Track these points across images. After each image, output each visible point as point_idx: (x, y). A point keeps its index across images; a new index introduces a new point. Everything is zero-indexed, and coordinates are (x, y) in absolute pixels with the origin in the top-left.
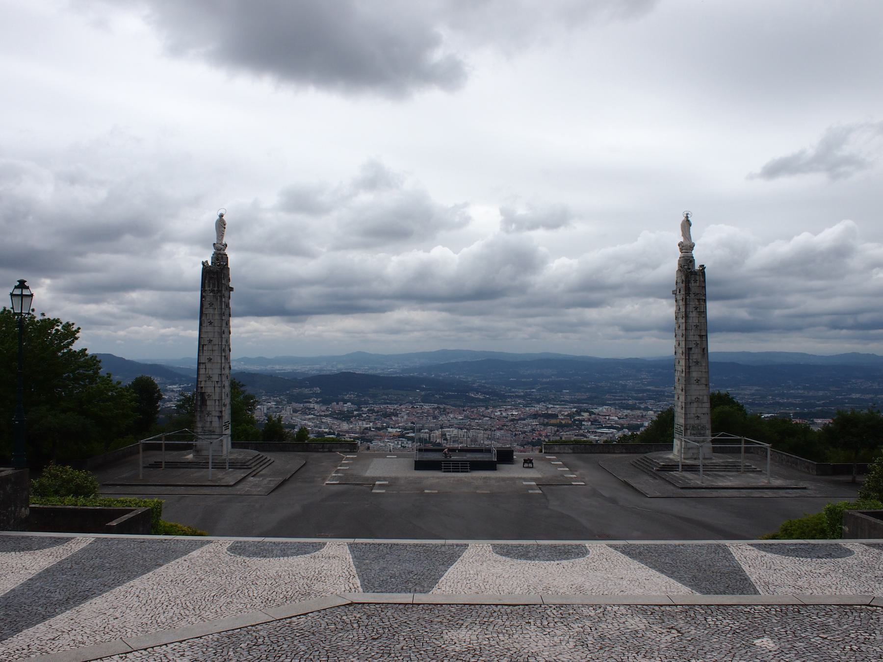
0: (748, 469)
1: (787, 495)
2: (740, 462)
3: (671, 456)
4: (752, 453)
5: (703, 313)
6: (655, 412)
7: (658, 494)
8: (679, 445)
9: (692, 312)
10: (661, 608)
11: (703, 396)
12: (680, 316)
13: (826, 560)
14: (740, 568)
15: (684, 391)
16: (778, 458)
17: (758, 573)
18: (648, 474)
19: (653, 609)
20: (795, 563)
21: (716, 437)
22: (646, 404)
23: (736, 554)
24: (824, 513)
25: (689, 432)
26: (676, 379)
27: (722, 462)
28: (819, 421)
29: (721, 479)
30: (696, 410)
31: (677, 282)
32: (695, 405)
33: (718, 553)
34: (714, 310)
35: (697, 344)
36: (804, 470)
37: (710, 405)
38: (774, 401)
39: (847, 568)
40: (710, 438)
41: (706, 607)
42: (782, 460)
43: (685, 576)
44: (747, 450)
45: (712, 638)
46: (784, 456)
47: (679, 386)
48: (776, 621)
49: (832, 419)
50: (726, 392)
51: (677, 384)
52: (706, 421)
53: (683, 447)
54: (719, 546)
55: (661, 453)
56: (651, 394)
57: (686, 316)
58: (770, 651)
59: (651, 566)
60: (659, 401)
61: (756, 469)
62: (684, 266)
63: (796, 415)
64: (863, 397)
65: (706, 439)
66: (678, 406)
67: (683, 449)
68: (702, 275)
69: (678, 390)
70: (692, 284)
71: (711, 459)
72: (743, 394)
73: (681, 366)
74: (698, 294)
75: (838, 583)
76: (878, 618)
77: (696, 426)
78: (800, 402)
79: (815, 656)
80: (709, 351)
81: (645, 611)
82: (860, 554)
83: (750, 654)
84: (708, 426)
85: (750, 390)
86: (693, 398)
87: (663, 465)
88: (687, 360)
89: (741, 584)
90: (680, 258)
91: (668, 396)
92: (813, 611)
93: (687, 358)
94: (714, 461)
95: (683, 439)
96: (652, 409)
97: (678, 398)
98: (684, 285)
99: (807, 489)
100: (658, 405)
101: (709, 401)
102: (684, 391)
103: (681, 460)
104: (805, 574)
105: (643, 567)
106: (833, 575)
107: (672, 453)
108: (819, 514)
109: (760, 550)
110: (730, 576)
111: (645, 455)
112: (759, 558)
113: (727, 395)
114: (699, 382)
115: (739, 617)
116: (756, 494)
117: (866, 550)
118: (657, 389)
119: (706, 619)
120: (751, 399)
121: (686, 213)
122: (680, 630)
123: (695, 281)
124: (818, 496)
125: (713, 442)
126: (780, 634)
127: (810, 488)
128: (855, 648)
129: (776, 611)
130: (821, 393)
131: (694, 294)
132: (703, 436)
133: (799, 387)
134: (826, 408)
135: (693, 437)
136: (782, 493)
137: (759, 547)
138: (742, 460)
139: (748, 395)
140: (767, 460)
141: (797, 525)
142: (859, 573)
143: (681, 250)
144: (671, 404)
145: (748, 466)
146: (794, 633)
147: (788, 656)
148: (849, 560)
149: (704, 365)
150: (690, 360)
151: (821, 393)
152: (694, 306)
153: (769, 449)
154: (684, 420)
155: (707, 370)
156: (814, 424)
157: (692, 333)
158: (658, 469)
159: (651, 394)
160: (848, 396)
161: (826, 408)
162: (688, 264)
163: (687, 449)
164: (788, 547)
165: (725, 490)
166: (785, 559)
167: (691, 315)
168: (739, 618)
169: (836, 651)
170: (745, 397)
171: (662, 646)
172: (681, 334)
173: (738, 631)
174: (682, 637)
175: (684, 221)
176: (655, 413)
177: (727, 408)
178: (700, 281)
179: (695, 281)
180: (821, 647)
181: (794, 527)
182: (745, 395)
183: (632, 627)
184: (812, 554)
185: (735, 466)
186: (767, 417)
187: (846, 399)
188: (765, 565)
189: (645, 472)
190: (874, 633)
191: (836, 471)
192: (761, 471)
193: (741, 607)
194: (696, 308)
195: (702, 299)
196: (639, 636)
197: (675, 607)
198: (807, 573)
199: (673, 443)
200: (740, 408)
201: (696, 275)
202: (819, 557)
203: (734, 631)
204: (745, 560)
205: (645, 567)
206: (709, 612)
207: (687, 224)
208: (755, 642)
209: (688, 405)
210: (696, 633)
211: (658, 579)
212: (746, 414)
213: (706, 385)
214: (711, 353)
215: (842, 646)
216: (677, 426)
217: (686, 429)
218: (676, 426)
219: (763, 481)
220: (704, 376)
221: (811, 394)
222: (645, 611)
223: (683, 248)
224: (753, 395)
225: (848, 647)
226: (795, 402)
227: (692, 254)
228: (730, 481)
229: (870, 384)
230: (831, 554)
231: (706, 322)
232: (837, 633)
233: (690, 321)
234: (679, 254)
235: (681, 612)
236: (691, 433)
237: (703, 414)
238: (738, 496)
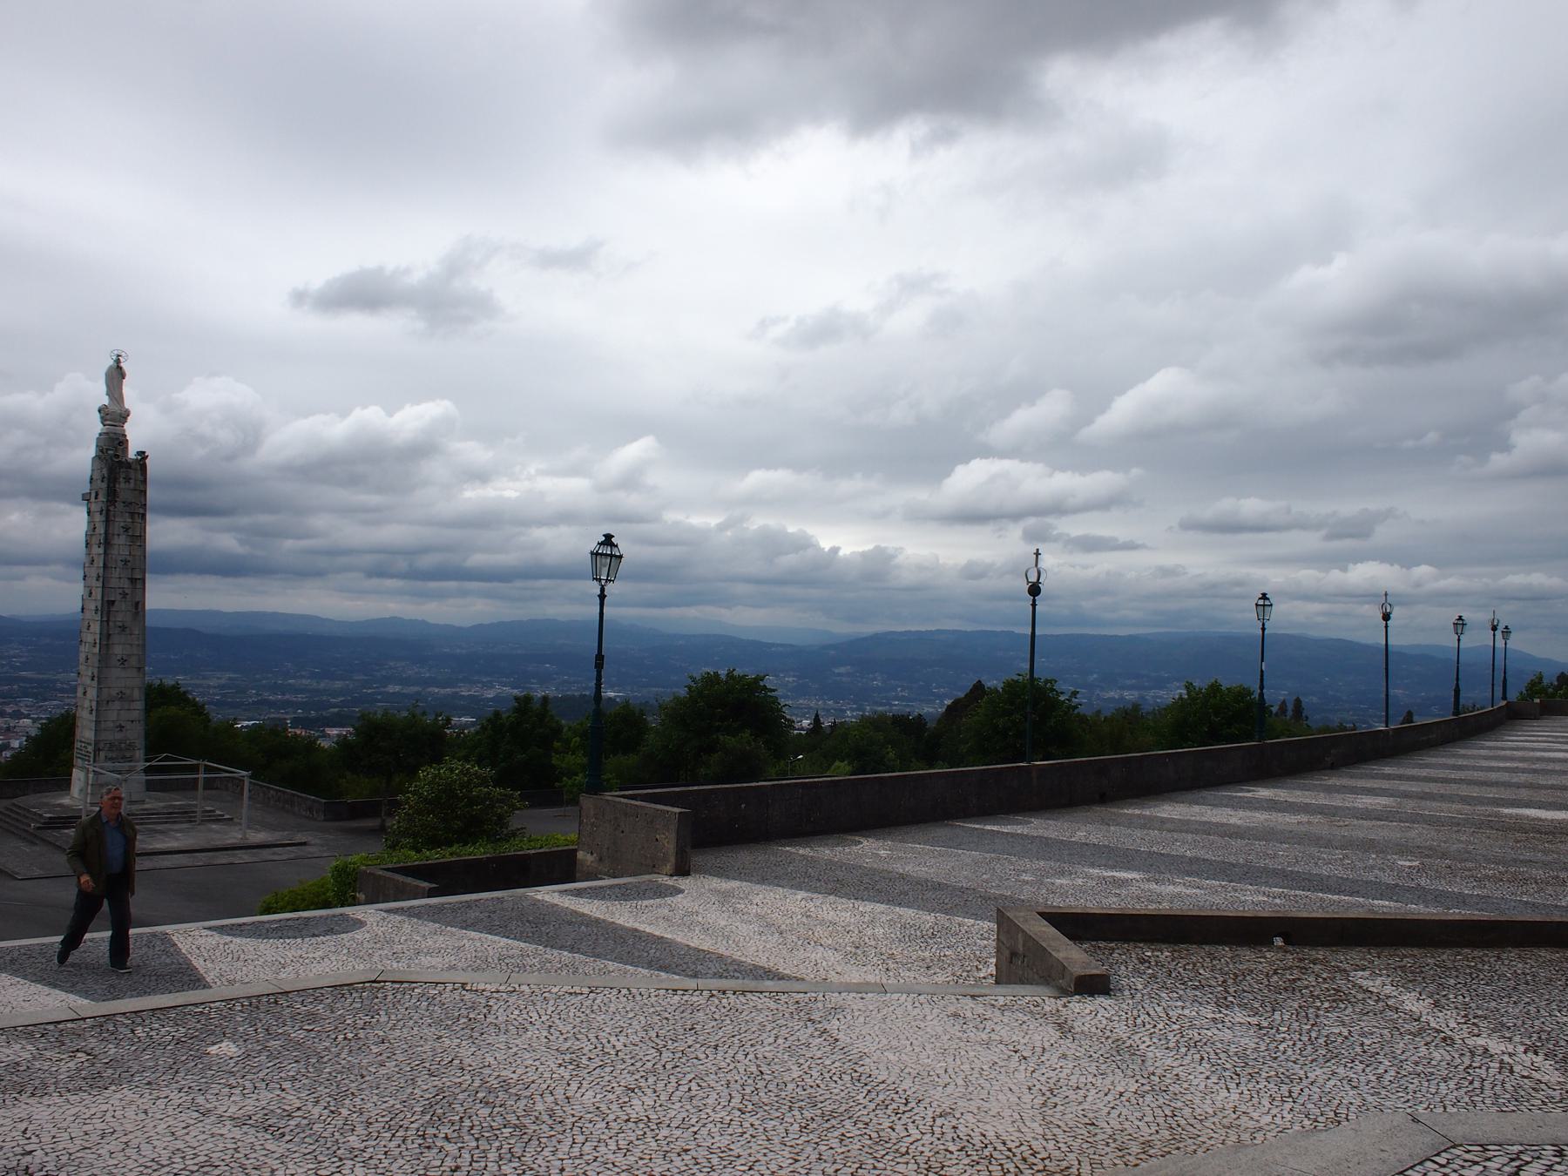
0: (210, 816)
1: (276, 858)
2: (196, 806)
3: (66, 801)
4: (217, 788)
5: (139, 539)
6: (34, 720)
7: (37, 872)
8: (82, 779)
9: (119, 535)
10: (59, 1026)
11: (133, 688)
12: (94, 540)
13: (325, 939)
14: (189, 963)
15: (96, 679)
16: (261, 795)
17: (218, 968)
18: (13, 833)
19: (45, 1029)
20: (277, 948)
21: (153, 763)
22: (16, 705)
23: (184, 944)
24: (330, 875)
25: (102, 754)
26: (82, 657)
27: (164, 808)
28: (334, 732)
29: (161, 837)
30: (118, 715)
31: (92, 479)
32: (117, 705)
33: (153, 946)
34: (162, 533)
35: (125, 595)
36: (304, 813)
37: (144, 705)
38: (260, 698)
39: (355, 945)
40: (142, 765)
41: (134, 1015)
42: (269, 798)
43: (96, 987)
44: (209, 784)
45: (143, 1055)
46: (272, 792)
47: (87, 672)
48: (241, 1019)
49: (353, 726)
50: (173, 683)
51: (82, 668)
52: (136, 734)
53: (90, 782)
54: (154, 935)
55: (47, 796)
56: (28, 685)
57: (107, 543)
58: (231, 1058)
59: (34, 979)
60: (45, 700)
61: (223, 815)
62: (107, 450)
63: (297, 722)
64: (404, 691)
65: (136, 766)
66: (83, 708)
67: (89, 787)
68: (141, 469)
69: (84, 677)
70: (121, 486)
71: (143, 802)
72: (206, 686)
73: (93, 634)
74: (131, 503)
75: (341, 968)
76: (386, 996)
77: (116, 743)
78: (304, 700)
79: (294, 1054)
80: (147, 607)
81: (31, 1034)
82: (375, 924)
83: (200, 1066)
84: (140, 743)
85: (218, 678)
86: (114, 692)
87: (50, 818)
88: (105, 624)
89: (188, 977)
90: (100, 434)
91: (62, 690)
92: (297, 999)
93: (105, 619)
94: (146, 806)
95: (91, 768)
96: (29, 715)
97: (85, 693)
98: (104, 485)
99: (310, 845)
100: (42, 706)
101: (143, 698)
102: (96, 679)
103: (85, 806)
104: (292, 961)
105: (19, 982)
106: (333, 958)
107: (69, 794)
108: (322, 879)
109: (222, 934)
110: (173, 979)
111: (15, 801)
112: (221, 946)
113: (176, 687)
114: (126, 663)
115: (186, 1021)
116: (223, 858)
117: (384, 919)
118: (41, 676)
119: (133, 1031)
120: (218, 695)
121: (116, 352)
122: (90, 1051)
123: (127, 480)
124: (325, 854)
125: (147, 771)
126: (247, 1035)
127: (313, 842)
128: (350, 1036)
129: (243, 1006)
130: (338, 684)
131: (124, 503)
132: (130, 761)
133: (303, 673)
134: (346, 709)
135: (109, 764)
136: (266, 854)
137: (221, 930)
138: (199, 802)
139: (215, 687)
140: (242, 799)
141: (286, 898)
142: (370, 951)
143: (103, 420)
144: (68, 704)
145: (210, 811)
146: (267, 1030)
147: (256, 1060)
148: (359, 935)
149: (137, 632)
150: (111, 623)
151: (338, 684)
152: (122, 524)
153: (247, 781)
154: (93, 733)
155: (141, 642)
156: (325, 737)
157: (116, 574)
158: (38, 825)
159: (28, 685)
160: (382, 689)
161: (346, 709)
162: (116, 448)
163: (98, 785)
164: (267, 926)
165: (170, 856)
166: (262, 942)
167: (117, 541)
168: (186, 1023)
169: (325, 1044)
170: (209, 692)
171: (62, 1077)
172: (96, 575)
173: (183, 1039)
174: (94, 1061)
175: (111, 367)
176: (34, 722)
177: (173, 710)
178: (135, 480)
179: (127, 480)
180: (304, 1042)
181: (281, 904)
182: (209, 687)
183: (9, 1058)
184: (304, 932)
185: (186, 812)
186: (247, 727)
187: (380, 694)
188: (230, 956)
189: (13, 833)
190: (378, 1014)
191: (357, 812)
192: (231, 819)
193: (190, 1007)
194: (126, 529)
195: (138, 512)
196: (21, 1069)
197: (82, 1022)
198: (295, 960)
199: (71, 775)
200: (199, 709)
201: (130, 468)
202: (314, 935)
203: (178, 1039)
204: (198, 951)
205: (22, 982)
206: (139, 1020)
207: (116, 375)
208: (209, 1049)
209: (101, 704)
210: (117, 1052)
211: (48, 998)
212: (209, 721)
213: (139, 668)
214: (150, 610)
215: (334, 1037)
216: (79, 744)
217: (97, 750)
218: (77, 745)
219: (234, 836)
220: (135, 652)
221: (322, 685)
222: (31, 1034)
223: (108, 417)
224: (222, 687)
225: (341, 1037)
226: (295, 699)
227: (124, 431)
228: (177, 839)
229: (416, 670)
230: (332, 929)
231: (145, 557)
232: (328, 1021)
233: (114, 551)
234: (98, 427)
235: (93, 1027)
236: (106, 757)
237: (132, 721)
238: (190, 864)
